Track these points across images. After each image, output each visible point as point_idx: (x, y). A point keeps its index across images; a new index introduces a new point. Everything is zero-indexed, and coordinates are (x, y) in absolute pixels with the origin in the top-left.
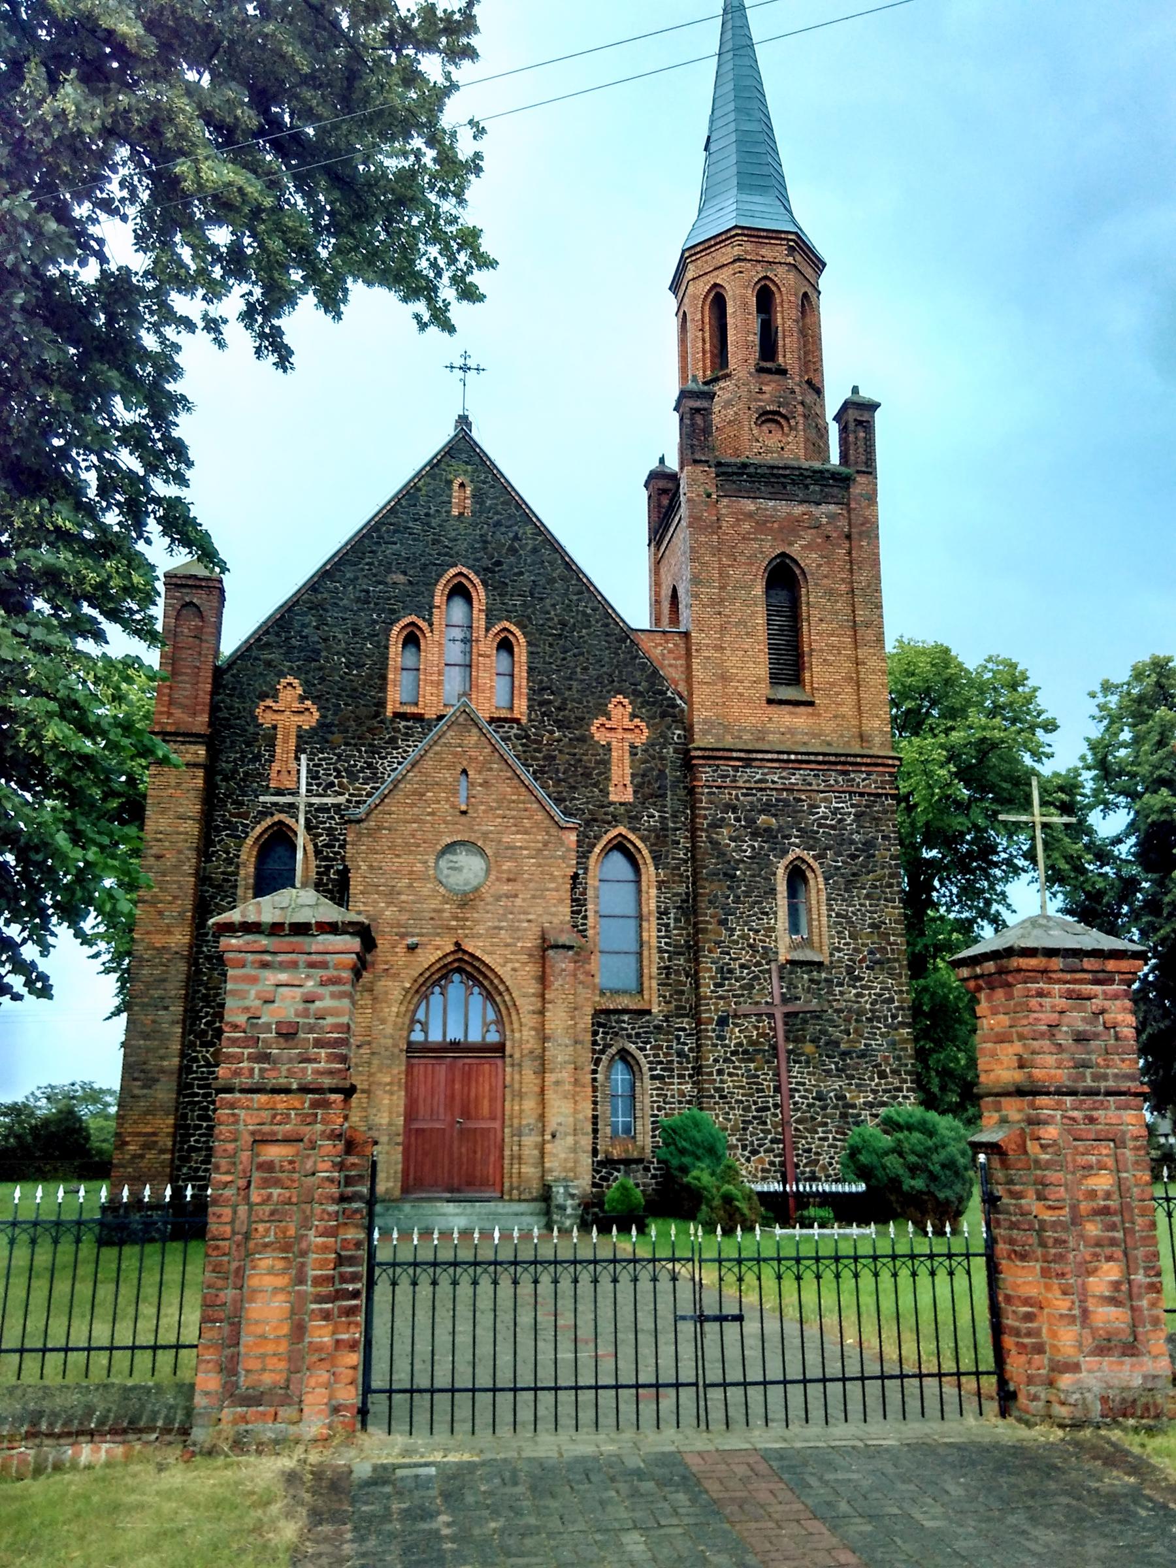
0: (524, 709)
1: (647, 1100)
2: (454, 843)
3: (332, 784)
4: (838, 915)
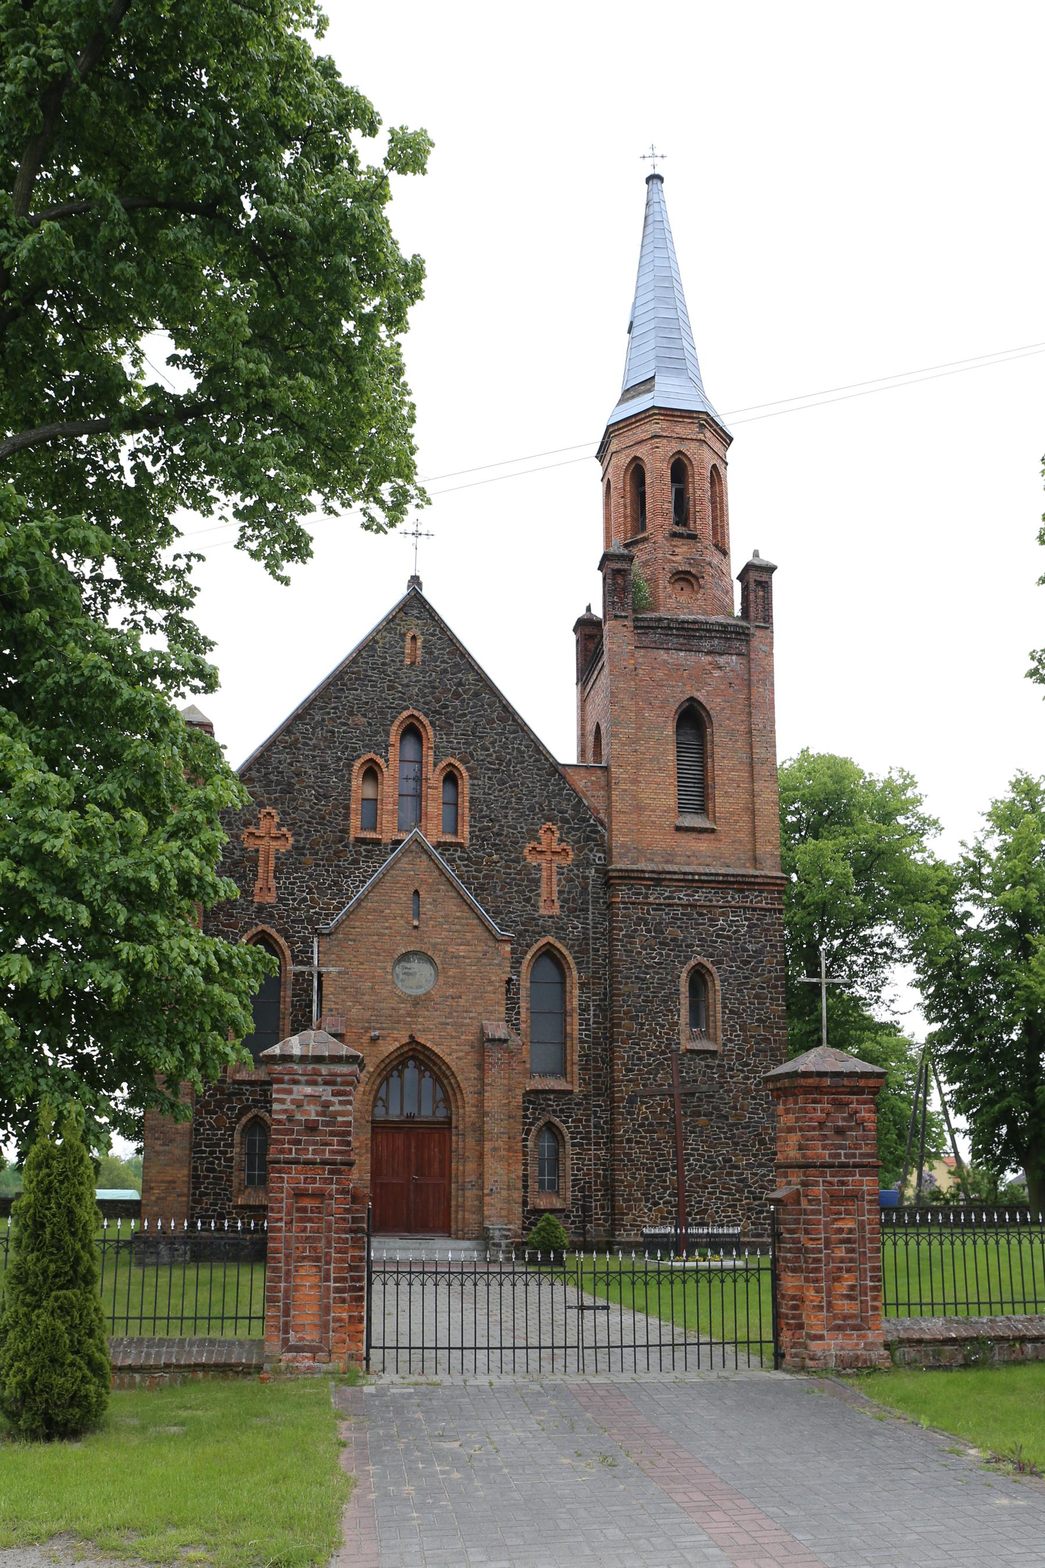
0: (467, 835)
2: (407, 953)
3: (305, 900)
4: (731, 1012)
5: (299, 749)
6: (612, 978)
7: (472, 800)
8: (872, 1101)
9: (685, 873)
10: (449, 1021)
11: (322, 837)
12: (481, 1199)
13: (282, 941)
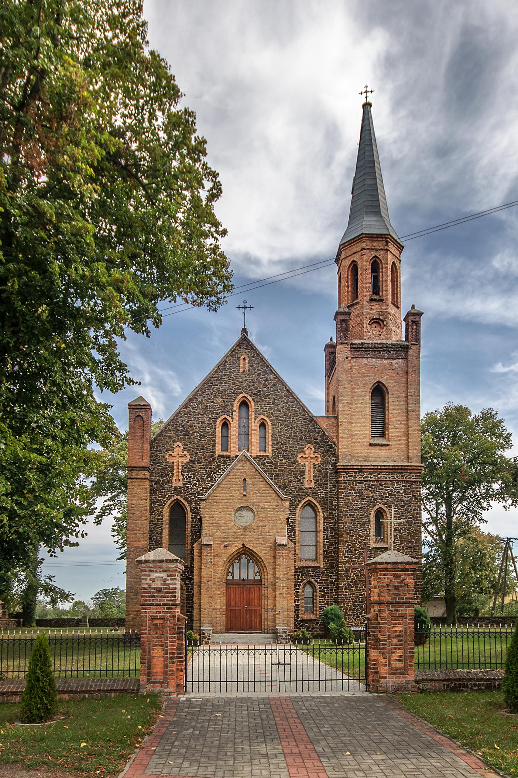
0: (270, 451)
1: (318, 599)
3: (196, 484)
5: (191, 415)
6: (338, 515)
7: (273, 435)
8: (412, 575)
9: (373, 466)
10: (260, 537)
11: (203, 455)
12: (275, 615)
13: (186, 503)
